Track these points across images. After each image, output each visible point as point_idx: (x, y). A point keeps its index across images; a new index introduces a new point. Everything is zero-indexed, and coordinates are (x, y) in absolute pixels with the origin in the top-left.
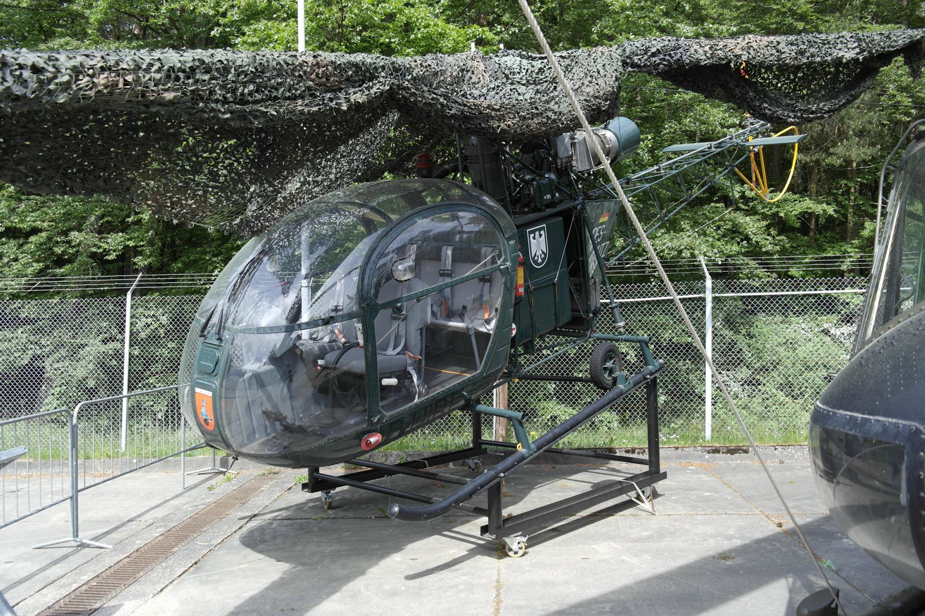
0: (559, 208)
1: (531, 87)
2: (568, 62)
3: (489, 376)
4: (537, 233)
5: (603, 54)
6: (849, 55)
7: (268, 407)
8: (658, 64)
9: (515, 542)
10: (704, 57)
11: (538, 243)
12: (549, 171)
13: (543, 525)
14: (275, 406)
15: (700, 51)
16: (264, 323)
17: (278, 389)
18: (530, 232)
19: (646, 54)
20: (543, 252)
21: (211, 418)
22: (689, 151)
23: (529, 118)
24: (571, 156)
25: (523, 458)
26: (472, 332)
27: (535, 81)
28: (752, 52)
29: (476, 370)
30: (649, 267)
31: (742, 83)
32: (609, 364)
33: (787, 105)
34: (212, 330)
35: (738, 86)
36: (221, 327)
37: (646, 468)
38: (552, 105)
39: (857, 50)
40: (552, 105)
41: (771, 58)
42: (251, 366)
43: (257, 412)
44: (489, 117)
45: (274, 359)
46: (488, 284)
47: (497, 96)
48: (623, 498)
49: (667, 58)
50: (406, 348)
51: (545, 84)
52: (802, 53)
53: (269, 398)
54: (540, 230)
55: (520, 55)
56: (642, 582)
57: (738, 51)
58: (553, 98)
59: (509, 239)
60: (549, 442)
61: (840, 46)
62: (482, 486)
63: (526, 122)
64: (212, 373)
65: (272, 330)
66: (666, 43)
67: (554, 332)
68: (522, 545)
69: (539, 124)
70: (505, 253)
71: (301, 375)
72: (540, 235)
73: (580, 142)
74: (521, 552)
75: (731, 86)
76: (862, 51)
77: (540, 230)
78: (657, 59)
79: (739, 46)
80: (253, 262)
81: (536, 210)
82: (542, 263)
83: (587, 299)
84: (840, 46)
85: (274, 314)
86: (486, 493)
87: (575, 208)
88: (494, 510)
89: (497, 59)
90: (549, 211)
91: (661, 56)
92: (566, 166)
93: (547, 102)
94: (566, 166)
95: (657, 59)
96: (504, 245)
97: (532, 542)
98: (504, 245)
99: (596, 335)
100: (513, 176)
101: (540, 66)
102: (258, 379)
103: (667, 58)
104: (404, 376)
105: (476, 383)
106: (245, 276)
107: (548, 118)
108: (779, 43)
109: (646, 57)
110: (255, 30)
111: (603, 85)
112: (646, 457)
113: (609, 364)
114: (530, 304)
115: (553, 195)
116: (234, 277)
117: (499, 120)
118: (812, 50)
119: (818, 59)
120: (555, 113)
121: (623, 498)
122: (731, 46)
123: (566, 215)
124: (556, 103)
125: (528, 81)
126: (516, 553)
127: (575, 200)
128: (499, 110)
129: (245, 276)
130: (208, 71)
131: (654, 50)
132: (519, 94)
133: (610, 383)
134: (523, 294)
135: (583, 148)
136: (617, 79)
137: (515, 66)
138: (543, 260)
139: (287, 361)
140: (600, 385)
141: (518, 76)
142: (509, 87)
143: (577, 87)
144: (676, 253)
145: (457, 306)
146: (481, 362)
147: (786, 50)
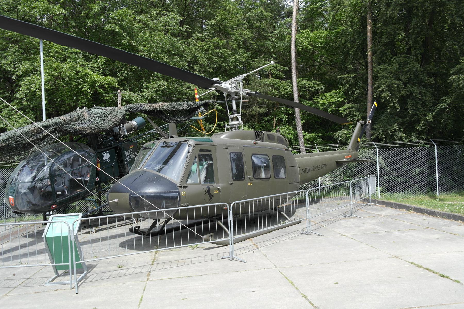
0: (113, 146)
6: (185, 108)
7: (28, 200)
11: (107, 156)
14: (29, 199)
16: (26, 181)
17: (31, 196)
21: (13, 203)
34: (13, 183)
36: (15, 182)
42: (23, 191)
43: (25, 202)
45: (29, 189)
50: (65, 185)
52: (174, 107)
53: (28, 198)
64: (13, 193)
65: (28, 182)
71: (36, 192)
78: (135, 110)
80: (23, 166)
85: (29, 178)
90: (110, 148)
95: (135, 110)
102: (25, 193)
104: (63, 192)
106: (22, 170)
110: (28, 79)
115: (111, 143)
116: (19, 170)
123: (116, 148)
129: (22, 170)
130: (11, 138)
139: (32, 189)
142: (93, 119)
145: (83, 173)
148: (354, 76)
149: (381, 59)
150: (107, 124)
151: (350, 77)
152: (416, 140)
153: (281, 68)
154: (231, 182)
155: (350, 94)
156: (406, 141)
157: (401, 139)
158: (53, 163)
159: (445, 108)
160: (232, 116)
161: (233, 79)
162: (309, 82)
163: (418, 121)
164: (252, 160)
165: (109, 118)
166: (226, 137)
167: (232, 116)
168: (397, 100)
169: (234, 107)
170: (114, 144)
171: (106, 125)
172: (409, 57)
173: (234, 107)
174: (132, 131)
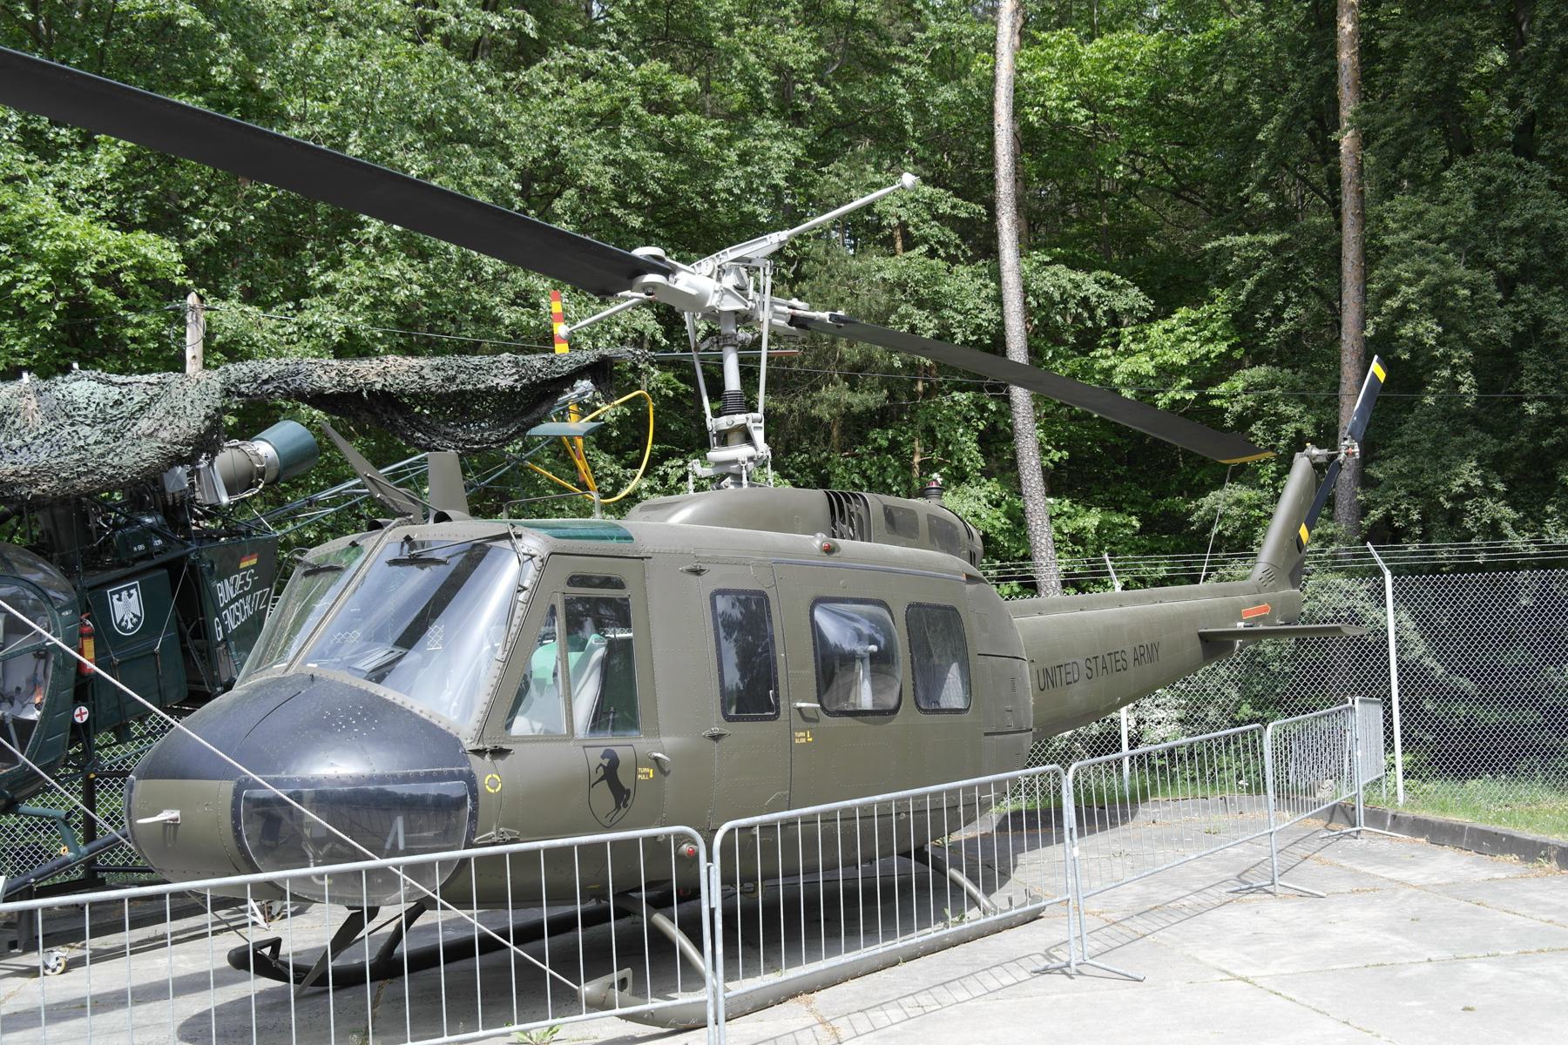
0: (157, 560)
2: (157, 390)
4: (124, 593)
6: (504, 383)
26: (9, 721)
28: (390, 379)
44: (13, 485)
52: (452, 379)
54: (128, 589)
59: (61, 610)
72: (130, 596)
74: (60, 969)
76: (522, 378)
77: (128, 589)
78: (270, 387)
81: (122, 565)
87: (187, 556)
92: (182, 503)
93: (102, 455)
94: (182, 503)
95: (270, 387)
115: (149, 545)
131: (265, 377)
136: (207, 417)
138: (136, 625)
142: (68, 429)
148: (1282, 242)
149: (1394, 167)
151: (1263, 244)
154: (716, 730)
155: (1260, 325)
160: (724, 422)
161: (729, 254)
164: (815, 626)
165: (144, 424)
166: (697, 520)
167: (724, 422)
169: (732, 381)
170: (163, 550)
173: (732, 381)
174: (251, 486)
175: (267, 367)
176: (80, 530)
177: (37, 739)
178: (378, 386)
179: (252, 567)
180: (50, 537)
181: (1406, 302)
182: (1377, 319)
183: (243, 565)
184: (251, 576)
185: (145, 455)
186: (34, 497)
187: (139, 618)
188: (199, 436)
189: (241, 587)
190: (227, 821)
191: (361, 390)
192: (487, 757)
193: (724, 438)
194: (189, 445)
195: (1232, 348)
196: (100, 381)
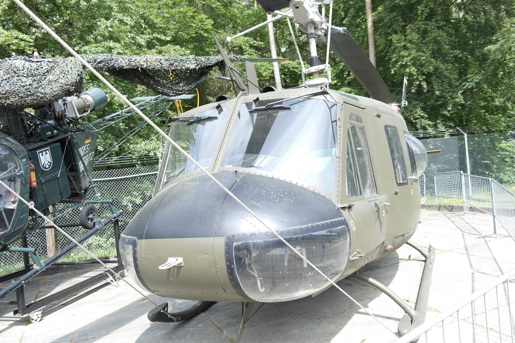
0: (57, 138)
1: (30, 78)
2: (53, 64)
3: (16, 232)
4: (44, 153)
5: (71, 61)
6: (192, 67)
8: (102, 67)
9: (35, 315)
10: (125, 65)
11: (46, 158)
12: (50, 119)
13: (51, 304)
15: (123, 61)
18: (39, 152)
19: (95, 62)
20: (49, 162)
22: (143, 101)
23: (25, 97)
24: (65, 110)
25: (37, 271)
27: (32, 75)
28: (148, 63)
29: (7, 229)
30: (135, 159)
31: (147, 77)
32: (91, 216)
33: (169, 87)
35: (145, 78)
37: (116, 265)
38: (40, 89)
39: (196, 64)
40: (40, 89)
41: (158, 66)
46: (13, 183)
47: (8, 84)
48: (104, 282)
49: (107, 64)
51: (39, 77)
52: (172, 65)
55: (25, 59)
56: (99, 319)
57: (142, 63)
58: (40, 86)
59: (21, 159)
60: (53, 261)
61: (188, 62)
62: (11, 290)
63: (24, 99)
66: (106, 57)
67: (62, 201)
68: (40, 316)
69: (32, 99)
70: (20, 166)
72: (46, 154)
73: (69, 103)
74: (39, 319)
75: (142, 78)
76: (198, 65)
79: (142, 60)
81: (42, 140)
82: (49, 168)
83: (80, 183)
84: (188, 62)
86: (15, 293)
87: (67, 137)
88: (20, 301)
89: (10, 61)
90: (50, 140)
91: (104, 64)
92: (62, 116)
94: (62, 116)
95: (101, 65)
96: (19, 162)
97: (45, 314)
98: (19, 162)
99: (87, 201)
100: (28, 122)
101: (36, 66)
103: (107, 64)
105: (7, 237)
107: (38, 96)
108: (161, 60)
109: (95, 64)
111: (70, 78)
112: (116, 259)
113: (91, 216)
114: (43, 190)
115: (52, 132)
117: (6, 99)
118: (176, 64)
119: (179, 68)
120: (42, 93)
121: (104, 282)
122: (138, 60)
123: (62, 142)
124: (43, 88)
125: (27, 74)
126: (36, 320)
127: (67, 133)
128: (5, 94)
131: (99, 60)
132: (22, 82)
133: (92, 225)
134: (36, 186)
135: (71, 106)
137: (20, 66)
138: (49, 166)
140: (85, 227)
141: (22, 72)
142: (16, 78)
143: (56, 79)
144: (147, 152)
146: (9, 224)
147: (164, 63)
150: (49, 89)
152: (443, 129)
153: (254, 43)
155: (345, 76)
156: (430, 130)
157: (424, 128)
158: (332, 287)
159: (472, 88)
162: (291, 62)
163: (444, 105)
165: (50, 77)
168: (425, 77)
169: (314, 52)
170: (58, 135)
171: (48, 90)
172: (428, 24)
173: (314, 52)
174: (85, 111)
175: (99, 56)
176: (31, 122)
177: (15, 217)
178: (145, 66)
179: (89, 143)
180: (8, 129)
181: (406, 62)
182: (395, 69)
183: (86, 142)
184: (89, 147)
185: (55, 90)
186: (8, 104)
187: (51, 163)
188: (76, 83)
189: (85, 151)
190: (222, 263)
191: (138, 68)
192: (346, 210)
193: (310, 75)
194: (73, 86)
195: (338, 82)
196: (26, 60)
